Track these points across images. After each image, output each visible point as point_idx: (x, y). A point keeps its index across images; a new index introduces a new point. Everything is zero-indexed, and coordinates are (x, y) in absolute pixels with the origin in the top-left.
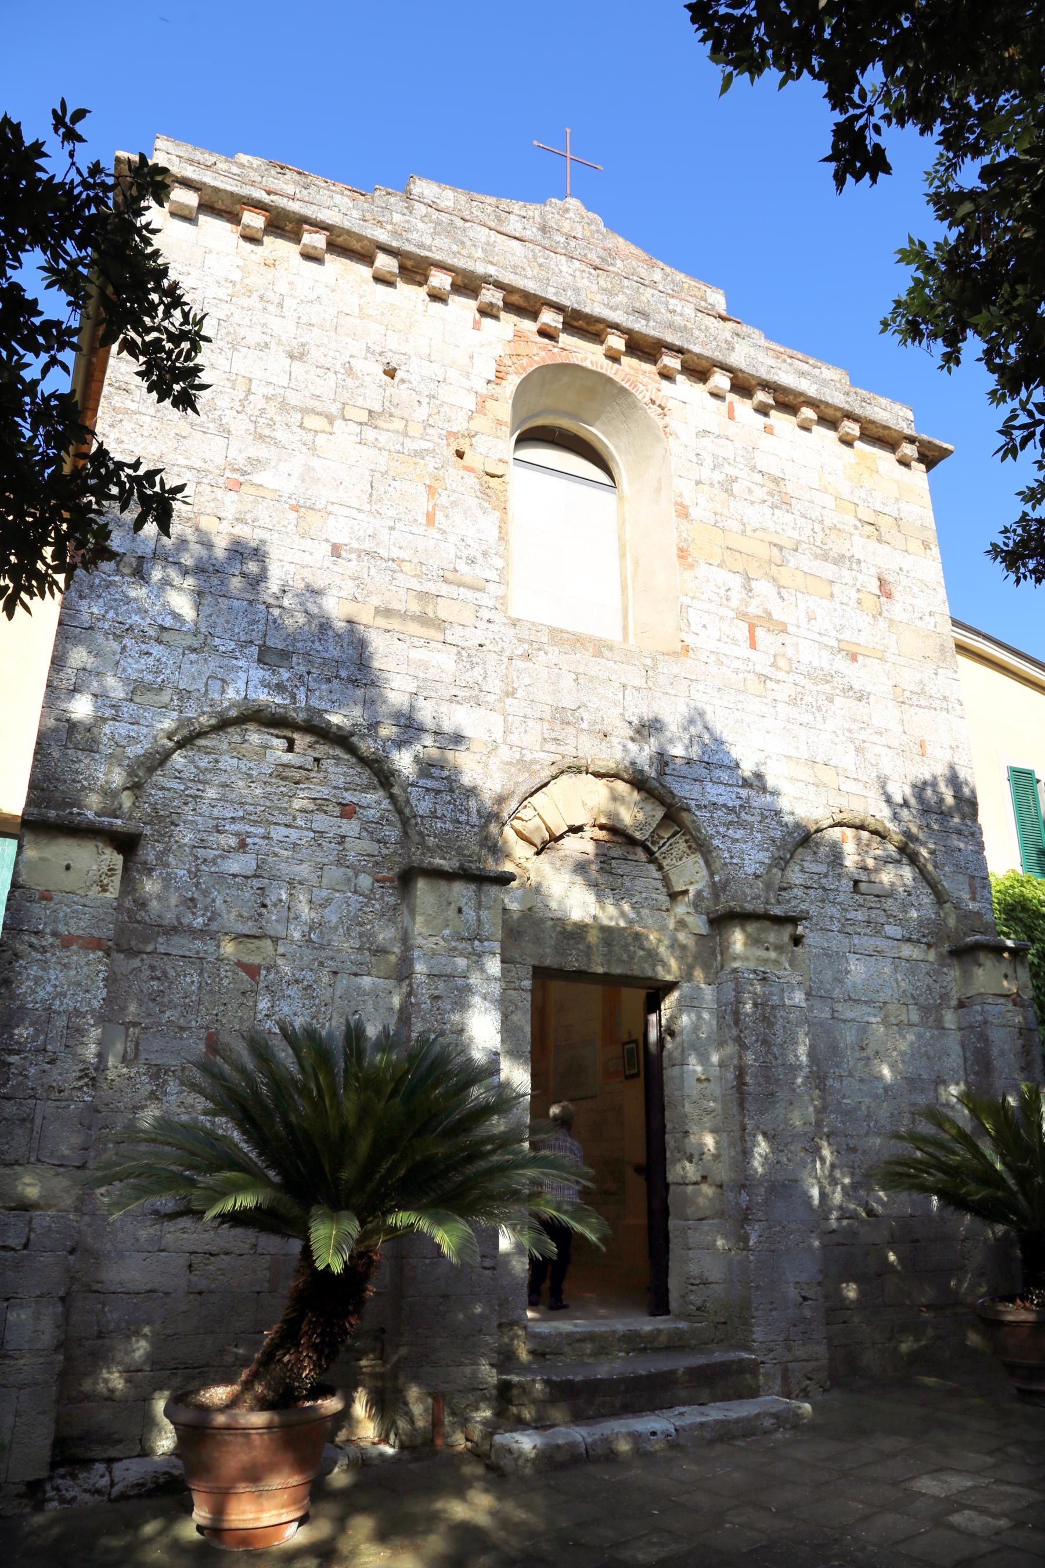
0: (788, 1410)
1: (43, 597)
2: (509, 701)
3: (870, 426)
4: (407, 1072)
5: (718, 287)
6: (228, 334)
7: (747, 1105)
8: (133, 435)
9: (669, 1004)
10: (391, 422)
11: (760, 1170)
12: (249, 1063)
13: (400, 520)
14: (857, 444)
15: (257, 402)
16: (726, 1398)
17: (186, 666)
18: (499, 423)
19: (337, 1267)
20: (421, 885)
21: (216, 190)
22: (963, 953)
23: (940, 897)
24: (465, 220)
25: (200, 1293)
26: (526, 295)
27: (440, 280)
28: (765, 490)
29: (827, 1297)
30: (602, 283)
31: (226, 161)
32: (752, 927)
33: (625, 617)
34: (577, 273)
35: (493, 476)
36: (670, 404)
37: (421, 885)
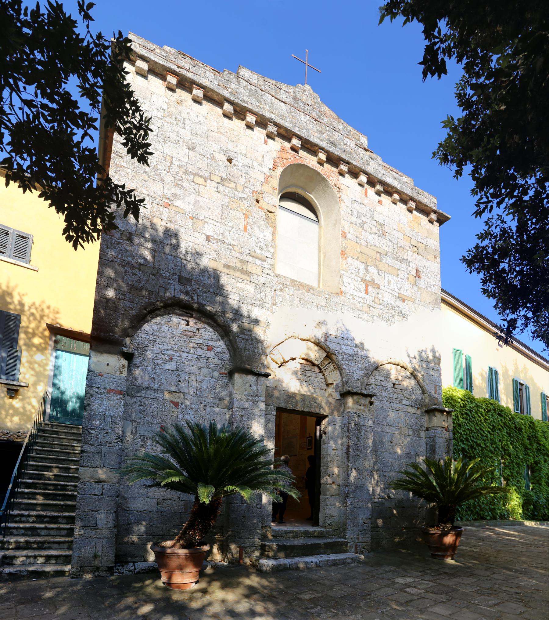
0: (356, 557)
1: (88, 242)
2: (274, 307)
3: (420, 204)
4: (232, 439)
5: (365, 135)
6: (162, 134)
7: (350, 459)
8: (125, 178)
9: (324, 422)
10: (230, 183)
11: (353, 481)
12: (175, 433)
13: (233, 228)
14: (414, 212)
15: (175, 168)
16: (336, 553)
17: (150, 281)
18: (274, 188)
19: (207, 502)
20: (237, 376)
21: (156, 63)
22: (430, 412)
23: (424, 392)
24: (262, 91)
25: (161, 512)
26: (286, 130)
27: (251, 118)
28: (377, 228)
29: (372, 523)
30: (318, 127)
31: (160, 49)
32: (355, 397)
33: (319, 278)
34: (308, 122)
35: (270, 212)
36: (342, 187)
37: (237, 376)
